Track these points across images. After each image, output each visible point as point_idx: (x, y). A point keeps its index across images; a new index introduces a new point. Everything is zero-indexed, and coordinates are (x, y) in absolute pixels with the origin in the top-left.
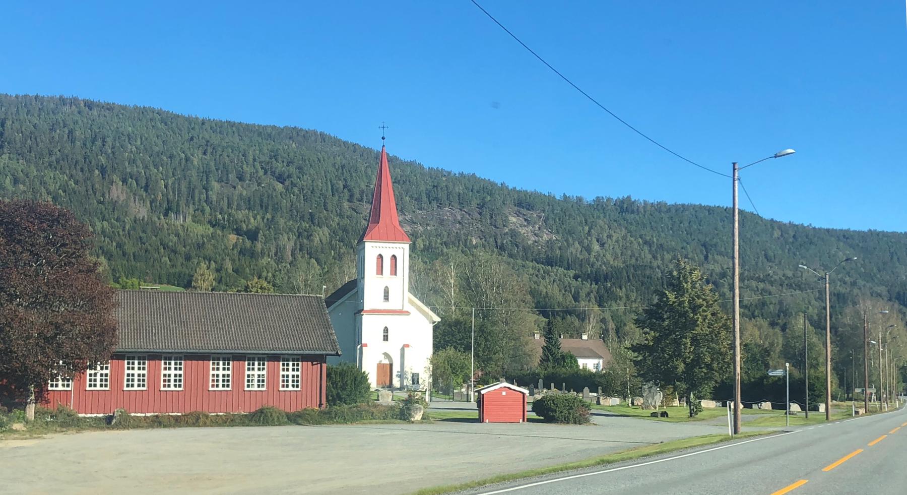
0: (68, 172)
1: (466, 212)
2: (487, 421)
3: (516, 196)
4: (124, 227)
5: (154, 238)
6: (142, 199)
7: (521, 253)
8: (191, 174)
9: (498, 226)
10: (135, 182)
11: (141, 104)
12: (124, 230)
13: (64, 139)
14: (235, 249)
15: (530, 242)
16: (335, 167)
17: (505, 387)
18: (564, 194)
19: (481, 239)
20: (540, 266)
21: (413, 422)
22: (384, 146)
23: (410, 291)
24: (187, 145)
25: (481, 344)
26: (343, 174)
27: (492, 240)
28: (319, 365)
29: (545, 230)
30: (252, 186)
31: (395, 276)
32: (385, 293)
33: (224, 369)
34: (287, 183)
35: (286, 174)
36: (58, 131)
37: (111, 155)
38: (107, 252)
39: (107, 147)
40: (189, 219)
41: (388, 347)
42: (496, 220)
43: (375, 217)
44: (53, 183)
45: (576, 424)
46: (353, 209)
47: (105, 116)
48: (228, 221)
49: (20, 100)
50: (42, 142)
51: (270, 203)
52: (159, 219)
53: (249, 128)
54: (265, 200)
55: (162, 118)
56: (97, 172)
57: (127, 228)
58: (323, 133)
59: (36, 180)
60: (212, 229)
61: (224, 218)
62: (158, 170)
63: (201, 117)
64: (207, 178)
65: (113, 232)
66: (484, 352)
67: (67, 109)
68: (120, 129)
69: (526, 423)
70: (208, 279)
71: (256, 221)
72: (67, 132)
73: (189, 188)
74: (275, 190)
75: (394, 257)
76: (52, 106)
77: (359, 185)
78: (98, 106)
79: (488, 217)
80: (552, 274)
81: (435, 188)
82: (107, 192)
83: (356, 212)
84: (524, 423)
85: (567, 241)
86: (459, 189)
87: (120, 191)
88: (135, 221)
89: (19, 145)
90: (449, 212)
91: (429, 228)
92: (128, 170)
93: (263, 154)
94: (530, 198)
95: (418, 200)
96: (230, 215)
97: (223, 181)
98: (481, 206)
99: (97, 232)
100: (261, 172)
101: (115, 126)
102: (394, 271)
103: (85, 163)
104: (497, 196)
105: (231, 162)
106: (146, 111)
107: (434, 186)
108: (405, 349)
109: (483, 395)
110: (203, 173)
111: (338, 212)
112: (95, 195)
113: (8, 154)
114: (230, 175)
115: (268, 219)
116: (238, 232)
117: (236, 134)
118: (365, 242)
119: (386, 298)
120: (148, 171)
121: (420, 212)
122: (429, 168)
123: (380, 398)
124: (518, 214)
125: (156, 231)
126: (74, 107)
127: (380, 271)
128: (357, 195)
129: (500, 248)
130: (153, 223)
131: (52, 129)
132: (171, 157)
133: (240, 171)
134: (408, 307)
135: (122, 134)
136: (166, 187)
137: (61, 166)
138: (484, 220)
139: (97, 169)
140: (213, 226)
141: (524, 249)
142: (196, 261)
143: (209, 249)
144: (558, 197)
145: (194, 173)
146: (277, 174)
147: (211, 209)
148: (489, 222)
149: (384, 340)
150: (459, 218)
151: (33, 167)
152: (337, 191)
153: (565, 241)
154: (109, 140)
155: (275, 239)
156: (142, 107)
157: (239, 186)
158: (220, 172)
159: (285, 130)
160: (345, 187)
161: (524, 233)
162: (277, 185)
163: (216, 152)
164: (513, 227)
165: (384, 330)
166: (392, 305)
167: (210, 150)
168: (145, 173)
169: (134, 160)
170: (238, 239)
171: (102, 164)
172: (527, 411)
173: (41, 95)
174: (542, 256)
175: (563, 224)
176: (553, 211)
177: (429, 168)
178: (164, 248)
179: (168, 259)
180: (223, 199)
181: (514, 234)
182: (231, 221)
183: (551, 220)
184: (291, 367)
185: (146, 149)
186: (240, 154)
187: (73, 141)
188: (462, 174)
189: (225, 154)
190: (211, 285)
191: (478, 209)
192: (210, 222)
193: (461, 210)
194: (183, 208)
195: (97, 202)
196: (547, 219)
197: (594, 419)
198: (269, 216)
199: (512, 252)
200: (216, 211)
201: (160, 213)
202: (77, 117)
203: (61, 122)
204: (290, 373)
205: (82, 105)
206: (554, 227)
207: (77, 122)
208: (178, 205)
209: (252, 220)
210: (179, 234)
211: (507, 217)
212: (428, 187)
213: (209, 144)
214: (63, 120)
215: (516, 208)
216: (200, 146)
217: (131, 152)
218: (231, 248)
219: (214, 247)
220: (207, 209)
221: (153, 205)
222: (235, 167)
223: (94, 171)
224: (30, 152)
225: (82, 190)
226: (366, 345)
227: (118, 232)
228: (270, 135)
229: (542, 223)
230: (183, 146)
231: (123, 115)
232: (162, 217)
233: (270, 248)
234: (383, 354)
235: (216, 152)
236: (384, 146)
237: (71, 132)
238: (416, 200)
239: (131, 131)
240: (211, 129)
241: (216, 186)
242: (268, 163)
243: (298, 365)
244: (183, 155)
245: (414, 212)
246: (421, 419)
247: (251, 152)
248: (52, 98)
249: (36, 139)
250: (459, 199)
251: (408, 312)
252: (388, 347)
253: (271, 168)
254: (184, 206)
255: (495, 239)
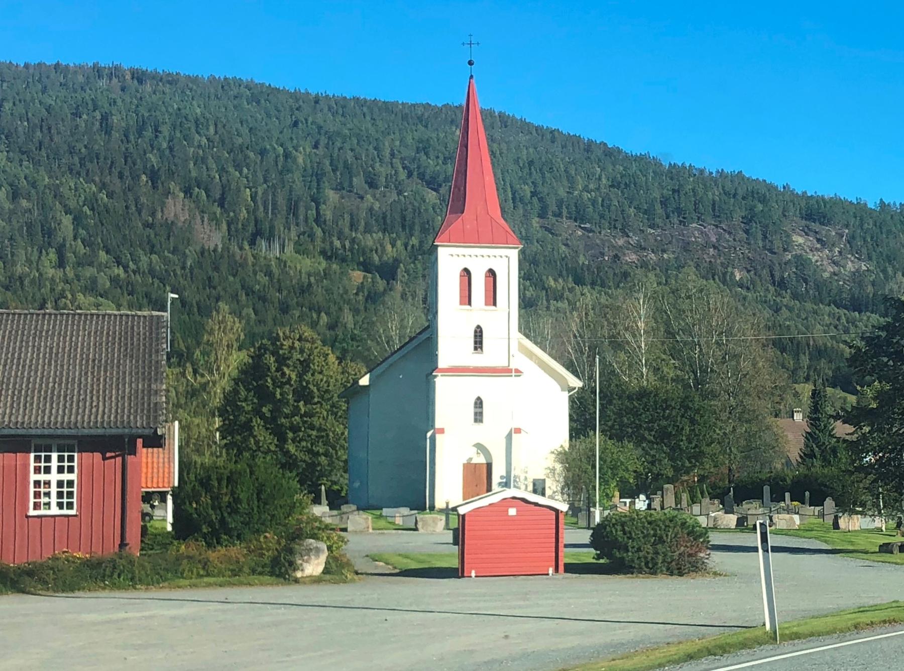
0: (97, 179)
1: (725, 230)
2: (473, 574)
3: (803, 204)
4: (184, 263)
5: (231, 278)
6: (214, 218)
7: (811, 292)
8: (292, 178)
9: (776, 250)
10: (203, 192)
11: (220, 74)
12: (183, 268)
13: (95, 129)
14: (361, 294)
15: (826, 275)
16: (518, 165)
17: (514, 498)
18: (881, 200)
19: (749, 271)
20: (842, 312)
21: (297, 581)
22: (471, 77)
23: (520, 330)
24: (287, 133)
25: (682, 429)
26: (531, 174)
27: (765, 273)
28: (119, 460)
29: (849, 256)
30: (388, 194)
31: (493, 308)
32: (475, 336)
33: (61, 470)
34: (443, 190)
35: (442, 177)
36: (85, 117)
37: (167, 152)
38: (156, 301)
39: (160, 139)
40: (289, 249)
41: (481, 434)
42: (771, 242)
43: (458, 204)
44: (75, 196)
45: (672, 574)
46: (547, 229)
47: (164, 93)
48: (351, 250)
49: (31, 71)
50: (59, 133)
51: (416, 221)
52: (241, 248)
53: (388, 107)
54: (409, 217)
55: (252, 94)
56: (144, 178)
57: (189, 264)
58: (504, 113)
59: (47, 191)
60: (324, 264)
61: (344, 246)
62: (241, 172)
63: (313, 92)
64: (318, 185)
65: (166, 271)
66: (690, 443)
67: (103, 83)
68: (183, 111)
69: (562, 575)
70: (232, 329)
71: (395, 249)
72: (99, 117)
73: (290, 200)
74: (424, 201)
75: (492, 273)
76: (81, 79)
77: (556, 191)
78: (153, 78)
79: (760, 236)
80: (860, 324)
81: (676, 194)
82: (159, 209)
83: (552, 234)
84: (558, 576)
85: (884, 271)
86: (714, 194)
87: (179, 207)
88: (202, 253)
89: (22, 139)
90: (698, 230)
91: (665, 256)
92: (194, 174)
93: (406, 146)
94: (825, 207)
95: (649, 212)
96: (353, 241)
97: (344, 189)
98: (748, 220)
99: (141, 271)
100: (403, 175)
101: (176, 106)
102: (492, 299)
103: (125, 164)
104: (774, 204)
105: (356, 159)
106: (229, 84)
107: (674, 191)
108: (514, 436)
109: (464, 516)
110: (312, 176)
111: (524, 234)
112: (140, 214)
113: (6, 153)
114: (354, 179)
115: (413, 246)
116: (366, 267)
117: (368, 118)
118: (437, 246)
119: (478, 343)
120: (224, 174)
121: (652, 231)
122: (670, 164)
123: (420, 526)
124: (806, 232)
125: (236, 268)
126: (115, 80)
127: (467, 298)
128: (553, 207)
129: (779, 285)
130: (232, 256)
131: (77, 114)
132: (263, 153)
133: (370, 172)
134: (519, 361)
135: (187, 120)
136: (253, 198)
137: (88, 171)
138: (752, 242)
139: (144, 173)
140: (328, 258)
141: (818, 287)
142: (297, 313)
143: (319, 295)
144: (871, 205)
145: (297, 176)
146: (427, 177)
147: (324, 232)
148: (761, 245)
149: (476, 421)
150: (714, 239)
151: (42, 172)
152: (521, 200)
153: (882, 271)
154: (165, 130)
155: (424, 276)
156: (222, 78)
157: (369, 196)
158: (338, 173)
159: (444, 109)
160: (534, 194)
161: (817, 261)
162: (428, 193)
163: (333, 144)
164: (799, 252)
165: (476, 403)
166: (492, 356)
167: (323, 141)
168: (220, 178)
169: (203, 159)
170: (364, 277)
171: (153, 166)
172: (566, 546)
173: (63, 63)
174: (844, 295)
175: (877, 245)
176: (861, 226)
177: (670, 164)
178: (247, 295)
179: (252, 311)
180: (342, 216)
181: (800, 262)
182: (355, 251)
183: (858, 239)
184: (54, 464)
185: (223, 142)
186: (371, 147)
187: (108, 133)
188: (721, 173)
189: (347, 146)
190: (238, 340)
191: (743, 225)
192: (323, 253)
193: (717, 226)
194: (280, 231)
195: (143, 224)
196: (853, 237)
197: (717, 559)
198: (414, 241)
199: (799, 291)
200: (331, 235)
201: (243, 240)
202: (116, 94)
203: (90, 102)
204: (54, 477)
205: (128, 77)
206: (864, 250)
207: (115, 102)
208: (272, 228)
209: (389, 247)
210: (271, 271)
211: (788, 236)
212: (665, 192)
213: (322, 132)
214: (92, 99)
215: (804, 222)
216: (308, 135)
217: (199, 146)
218: (355, 291)
219: (326, 290)
220: (319, 232)
221: (232, 227)
222: (362, 167)
223: (139, 177)
224: (40, 149)
225: (119, 206)
226: (442, 431)
227: (174, 271)
228: (420, 119)
229: (845, 245)
230: (281, 136)
231: (191, 90)
232: (247, 247)
233: (415, 292)
234: (474, 446)
235: (333, 144)
236: (471, 77)
237: (105, 118)
238: (645, 212)
239: (199, 113)
240: (329, 110)
241: (332, 196)
242: (414, 159)
243: (71, 459)
244: (280, 150)
245: (643, 231)
246: (323, 573)
247: (387, 144)
248: (81, 67)
249: (49, 129)
250: (714, 210)
251: (517, 371)
252: (481, 434)
253: (419, 167)
254: (282, 229)
255: (771, 272)
